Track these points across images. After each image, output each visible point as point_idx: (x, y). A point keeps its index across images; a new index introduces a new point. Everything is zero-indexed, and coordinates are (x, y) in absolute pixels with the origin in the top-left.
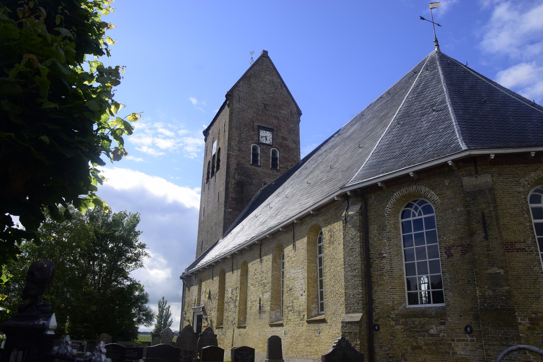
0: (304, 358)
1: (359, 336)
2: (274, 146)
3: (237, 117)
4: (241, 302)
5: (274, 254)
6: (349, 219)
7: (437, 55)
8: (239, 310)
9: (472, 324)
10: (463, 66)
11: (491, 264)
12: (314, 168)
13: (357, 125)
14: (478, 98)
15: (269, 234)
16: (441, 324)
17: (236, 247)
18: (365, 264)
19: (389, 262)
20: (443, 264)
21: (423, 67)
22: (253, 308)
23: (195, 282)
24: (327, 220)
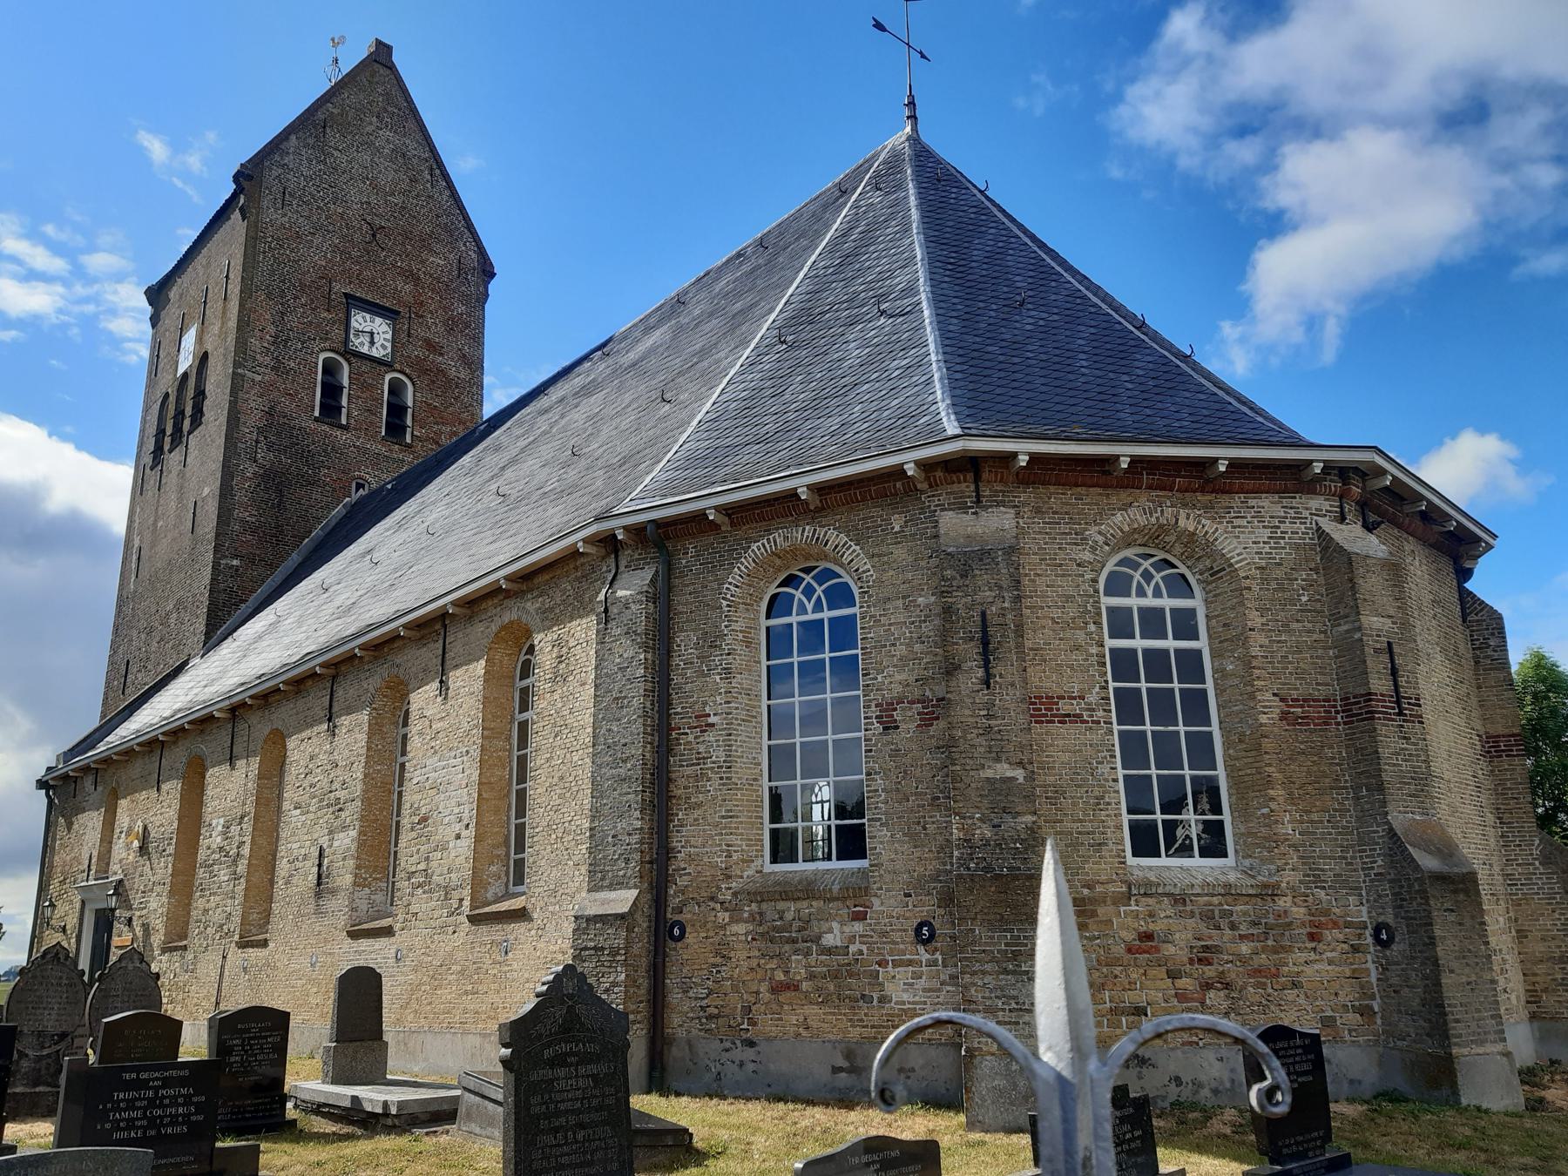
0: (453, 1030)
1: (623, 957)
3: (273, 256)
4: (254, 862)
5: (375, 709)
6: (615, 611)
7: (910, 146)
8: (246, 889)
9: (934, 918)
10: (976, 192)
11: (994, 755)
12: (523, 450)
13: (662, 330)
14: (1005, 289)
15: (363, 647)
16: (853, 920)
17: (250, 683)
18: (656, 744)
19: (723, 741)
20: (871, 751)
21: (867, 177)
22: (295, 880)
23: (95, 797)
24: (551, 609)
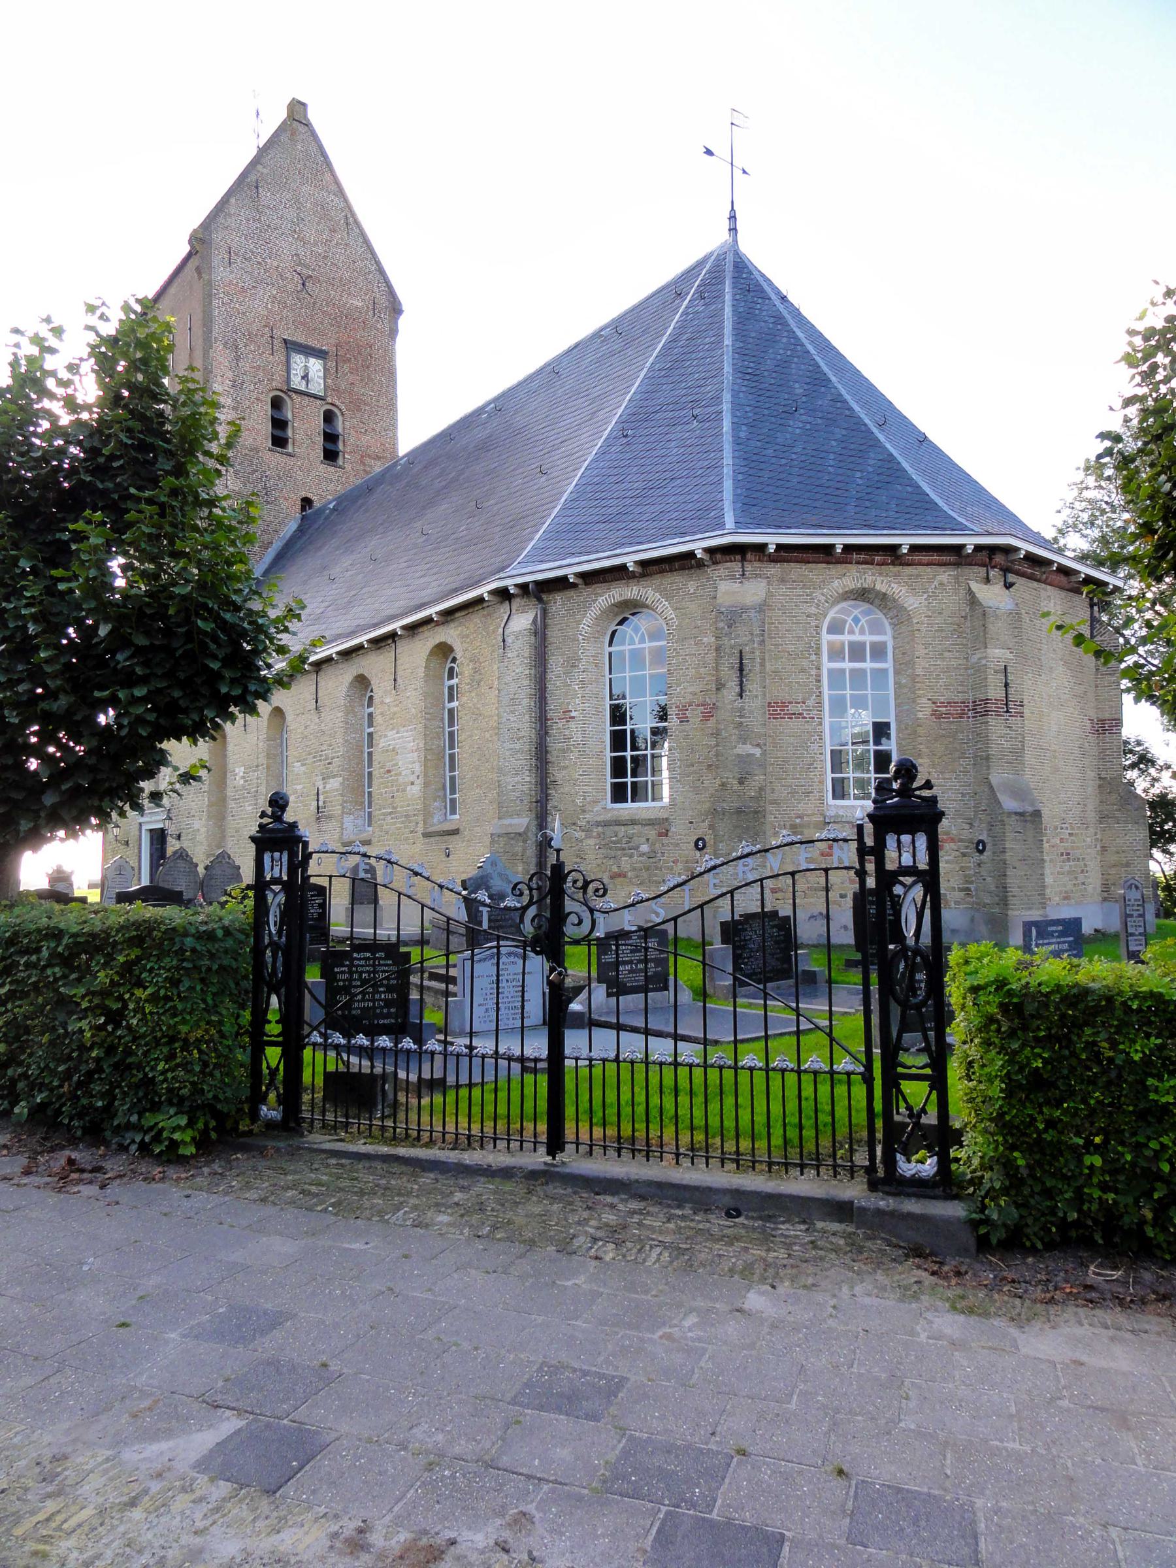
2: (329, 400)
14: (786, 396)
24: (467, 636)
